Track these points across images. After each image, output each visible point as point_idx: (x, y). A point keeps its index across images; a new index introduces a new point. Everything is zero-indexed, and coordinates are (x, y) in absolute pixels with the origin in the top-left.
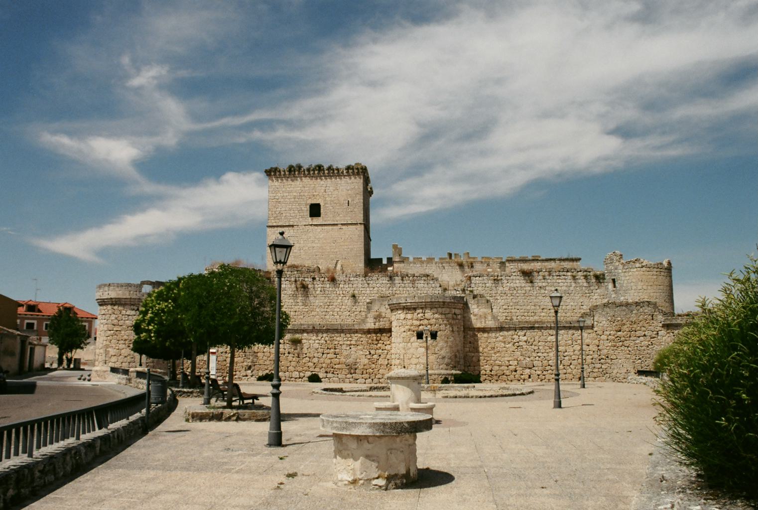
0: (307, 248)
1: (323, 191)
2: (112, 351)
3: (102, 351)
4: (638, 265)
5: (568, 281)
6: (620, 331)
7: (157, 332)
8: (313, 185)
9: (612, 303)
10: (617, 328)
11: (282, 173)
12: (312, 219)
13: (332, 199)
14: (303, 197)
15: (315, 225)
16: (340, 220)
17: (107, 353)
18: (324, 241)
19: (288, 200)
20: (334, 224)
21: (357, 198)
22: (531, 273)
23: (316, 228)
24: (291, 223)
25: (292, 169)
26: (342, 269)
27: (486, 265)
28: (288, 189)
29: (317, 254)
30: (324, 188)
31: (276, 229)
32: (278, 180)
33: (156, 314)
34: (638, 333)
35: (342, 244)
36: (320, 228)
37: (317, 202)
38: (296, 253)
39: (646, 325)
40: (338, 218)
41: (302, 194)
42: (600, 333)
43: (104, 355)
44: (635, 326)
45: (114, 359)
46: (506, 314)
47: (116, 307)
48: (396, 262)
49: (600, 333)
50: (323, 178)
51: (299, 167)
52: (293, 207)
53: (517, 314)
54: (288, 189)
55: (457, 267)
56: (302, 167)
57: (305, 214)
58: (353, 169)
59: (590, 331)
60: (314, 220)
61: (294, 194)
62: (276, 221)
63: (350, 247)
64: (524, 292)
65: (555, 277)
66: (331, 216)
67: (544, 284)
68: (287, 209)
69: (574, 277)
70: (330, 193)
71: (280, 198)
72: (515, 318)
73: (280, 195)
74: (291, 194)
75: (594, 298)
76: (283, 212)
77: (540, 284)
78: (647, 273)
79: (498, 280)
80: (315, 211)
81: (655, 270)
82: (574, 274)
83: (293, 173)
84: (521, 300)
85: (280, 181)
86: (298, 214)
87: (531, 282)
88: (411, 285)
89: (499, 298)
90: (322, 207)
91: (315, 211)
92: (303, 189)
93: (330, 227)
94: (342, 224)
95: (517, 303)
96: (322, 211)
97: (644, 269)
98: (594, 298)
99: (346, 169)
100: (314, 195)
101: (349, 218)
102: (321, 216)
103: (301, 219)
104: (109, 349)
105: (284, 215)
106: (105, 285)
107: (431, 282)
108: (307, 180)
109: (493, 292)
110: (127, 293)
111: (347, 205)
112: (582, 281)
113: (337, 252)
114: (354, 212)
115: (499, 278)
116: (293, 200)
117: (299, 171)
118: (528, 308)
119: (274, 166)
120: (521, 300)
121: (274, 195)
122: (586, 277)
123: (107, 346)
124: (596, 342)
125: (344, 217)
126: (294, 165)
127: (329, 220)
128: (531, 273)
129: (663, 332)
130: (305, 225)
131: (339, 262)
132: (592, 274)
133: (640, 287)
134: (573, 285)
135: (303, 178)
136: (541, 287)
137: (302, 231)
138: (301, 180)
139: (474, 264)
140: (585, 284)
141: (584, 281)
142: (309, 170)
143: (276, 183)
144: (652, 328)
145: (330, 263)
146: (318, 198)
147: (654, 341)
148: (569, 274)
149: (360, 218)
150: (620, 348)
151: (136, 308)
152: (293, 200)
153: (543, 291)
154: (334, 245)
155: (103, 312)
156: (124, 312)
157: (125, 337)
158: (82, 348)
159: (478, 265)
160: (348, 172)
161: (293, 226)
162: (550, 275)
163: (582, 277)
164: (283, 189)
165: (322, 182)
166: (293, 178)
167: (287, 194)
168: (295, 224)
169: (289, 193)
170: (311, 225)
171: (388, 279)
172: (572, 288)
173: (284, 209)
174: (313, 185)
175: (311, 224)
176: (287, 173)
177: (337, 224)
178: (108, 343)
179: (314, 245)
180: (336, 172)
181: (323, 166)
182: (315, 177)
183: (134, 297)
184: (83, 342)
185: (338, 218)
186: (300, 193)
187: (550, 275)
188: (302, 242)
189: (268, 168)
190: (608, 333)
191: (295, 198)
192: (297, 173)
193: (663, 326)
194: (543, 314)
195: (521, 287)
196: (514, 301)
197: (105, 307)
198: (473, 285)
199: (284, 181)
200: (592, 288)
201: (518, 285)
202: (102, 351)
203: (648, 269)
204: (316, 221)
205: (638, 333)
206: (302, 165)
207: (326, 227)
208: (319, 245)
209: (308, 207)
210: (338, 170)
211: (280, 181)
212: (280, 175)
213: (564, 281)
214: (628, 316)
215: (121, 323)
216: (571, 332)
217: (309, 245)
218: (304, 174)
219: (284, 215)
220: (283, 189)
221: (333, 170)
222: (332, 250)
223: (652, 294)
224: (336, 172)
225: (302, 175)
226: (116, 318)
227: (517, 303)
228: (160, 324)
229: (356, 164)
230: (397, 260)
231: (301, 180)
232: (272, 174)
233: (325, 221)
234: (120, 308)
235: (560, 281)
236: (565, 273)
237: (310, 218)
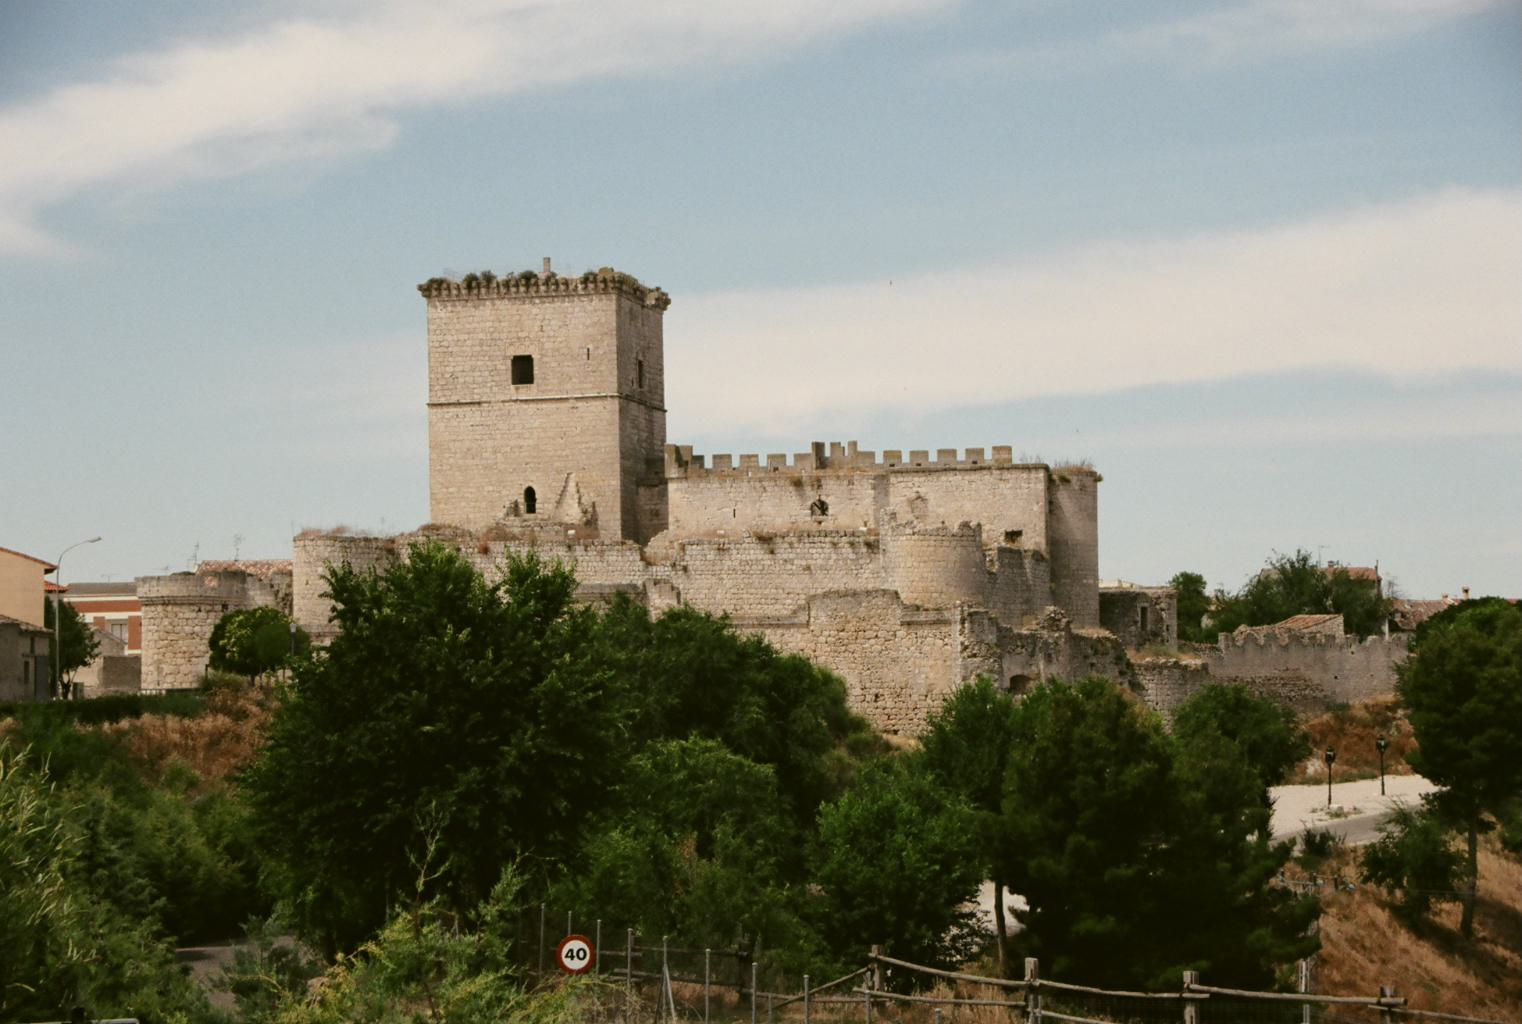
0: (508, 449)
1: (537, 329)
2: (166, 668)
3: (151, 668)
4: (908, 531)
5: (826, 550)
6: (843, 630)
7: (240, 653)
8: (518, 317)
9: (835, 592)
10: (840, 627)
11: (454, 292)
12: (517, 389)
13: (557, 345)
14: (498, 342)
15: (521, 401)
16: (572, 389)
17: (159, 670)
18: (542, 435)
19: (468, 349)
20: (561, 399)
21: (605, 343)
22: (771, 539)
23: (525, 406)
24: (476, 398)
25: (474, 284)
26: (578, 492)
27: (846, 482)
28: (468, 326)
29: (528, 460)
30: (539, 323)
31: (445, 409)
32: (445, 307)
33: (238, 639)
34: (869, 634)
35: (578, 439)
36: (533, 406)
37: (527, 353)
38: (487, 459)
39: (880, 623)
40: (569, 386)
41: (496, 335)
42: (817, 633)
43: (156, 673)
44: (864, 624)
45: (169, 679)
46: (734, 601)
47: (169, 608)
48: (672, 479)
49: (817, 633)
50: (537, 301)
51: (489, 278)
52: (479, 363)
53: (751, 601)
54: (468, 326)
55: (791, 488)
56: (495, 277)
57: (503, 378)
58: (595, 281)
59: (804, 630)
60: (521, 390)
61: (481, 336)
62: (446, 393)
63: (593, 445)
64: (760, 567)
65: (808, 545)
66: (555, 381)
67: (791, 556)
68: (467, 368)
69: (834, 545)
70: (552, 334)
71: (453, 344)
72: (746, 607)
73: (450, 338)
74: (475, 336)
75: (866, 576)
76: (459, 375)
77: (785, 556)
78: (920, 543)
79: (723, 550)
80: (523, 370)
81: (933, 538)
82: (836, 540)
83: (475, 291)
84: (755, 580)
85: (449, 309)
86: (490, 379)
87: (772, 552)
88: (598, 558)
89: (725, 576)
90: (535, 363)
91: (523, 370)
92: (497, 325)
93: (554, 406)
94: (576, 398)
95: (750, 584)
96: (536, 372)
97: (916, 537)
98: (866, 576)
99: (582, 283)
100: (519, 338)
101: (590, 385)
102: (535, 381)
103: (495, 389)
104: (163, 666)
105: (461, 380)
106: (152, 578)
107: (628, 553)
108: (504, 307)
109: (717, 568)
110: (185, 590)
111: (585, 357)
112: (847, 551)
113: (567, 456)
114: (598, 374)
115: (726, 546)
116: (478, 348)
117: (488, 287)
118: (767, 592)
119: (438, 275)
120: (755, 580)
121: (440, 338)
122: (852, 544)
123: (159, 662)
124: (813, 646)
125: (580, 382)
126: (478, 274)
127: (550, 391)
128: (771, 539)
129: (902, 633)
130: (503, 402)
131: (573, 476)
132: (861, 540)
133: (909, 565)
134: (834, 557)
135: (498, 302)
136: (786, 561)
137: (498, 413)
138: (494, 305)
139: (823, 482)
140: (852, 556)
141: (850, 550)
142: (507, 284)
143: (442, 312)
144: (887, 627)
145: (554, 480)
146: (527, 343)
147: (890, 644)
148: (828, 539)
149: (608, 380)
150: (843, 655)
151: (197, 609)
152: (478, 348)
153: (789, 566)
154: (562, 441)
155: (151, 615)
156: (181, 615)
157: (184, 648)
158: (85, 664)
159: (832, 482)
160: (585, 288)
161: (479, 403)
162: (799, 541)
163: (847, 546)
164: (458, 326)
165: (535, 311)
166: (477, 302)
167: (466, 337)
168: (484, 399)
169: (469, 333)
170: (516, 401)
171: (566, 549)
172: (831, 562)
173: (461, 368)
174: (518, 317)
175: (514, 398)
176: (464, 292)
177: (567, 399)
178: (160, 657)
179: (521, 442)
180: (562, 287)
181: (535, 276)
182: (520, 299)
183: (194, 594)
184: (89, 654)
185: (569, 386)
186: (492, 333)
187: (799, 541)
188: (499, 437)
189: (424, 281)
190: (826, 633)
191: (481, 345)
192: (483, 291)
193: (902, 624)
194: (789, 601)
195: (757, 560)
196: (746, 581)
197: (153, 608)
198: (687, 558)
199: (459, 308)
200: (861, 562)
201: (753, 557)
202: (151, 668)
203: (922, 537)
204: (526, 392)
205: (869, 634)
206: (494, 272)
207: (544, 406)
208: (531, 442)
209: (509, 362)
210: (566, 283)
211: (449, 309)
212: (449, 295)
213: (820, 550)
214: (854, 610)
215: (178, 629)
216: (779, 631)
217: (512, 443)
218: (499, 292)
219: (461, 380)
220: (458, 326)
221: (557, 283)
222: (559, 452)
223: (925, 575)
224: (562, 287)
225: (495, 296)
226: (171, 624)
227: (750, 584)
228: (242, 646)
229: (601, 270)
230: (673, 476)
231: (494, 305)
232: (434, 293)
233: (543, 392)
234: (176, 609)
235: (814, 551)
236: (822, 539)
237: (512, 387)
